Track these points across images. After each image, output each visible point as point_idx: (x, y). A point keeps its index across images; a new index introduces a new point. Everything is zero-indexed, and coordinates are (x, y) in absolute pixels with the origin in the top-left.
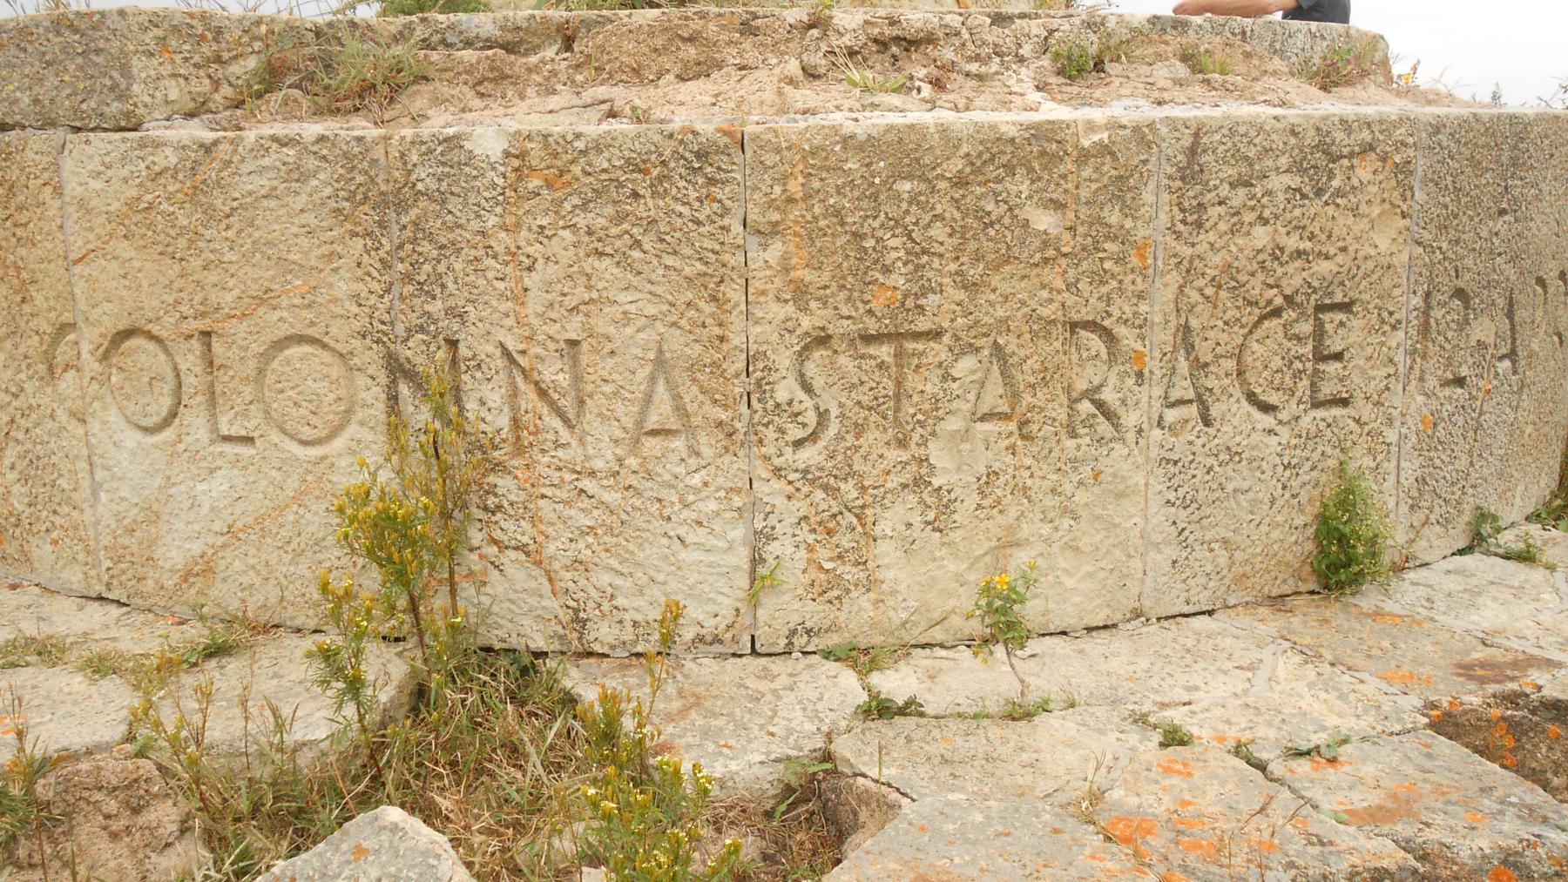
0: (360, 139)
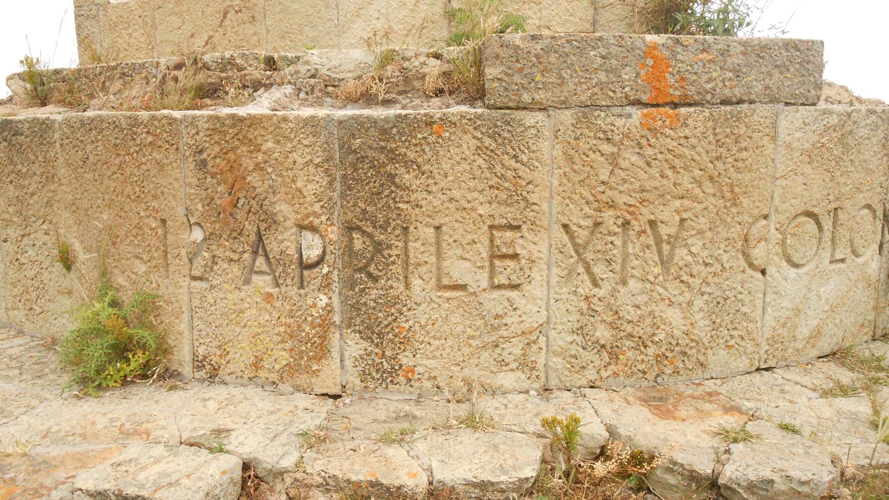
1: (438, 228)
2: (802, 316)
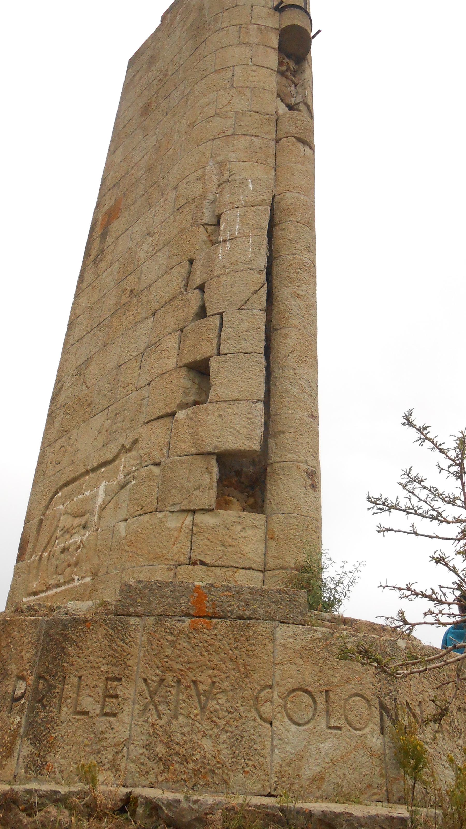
0: (374, 637)
1: (80, 678)
2: (305, 761)
